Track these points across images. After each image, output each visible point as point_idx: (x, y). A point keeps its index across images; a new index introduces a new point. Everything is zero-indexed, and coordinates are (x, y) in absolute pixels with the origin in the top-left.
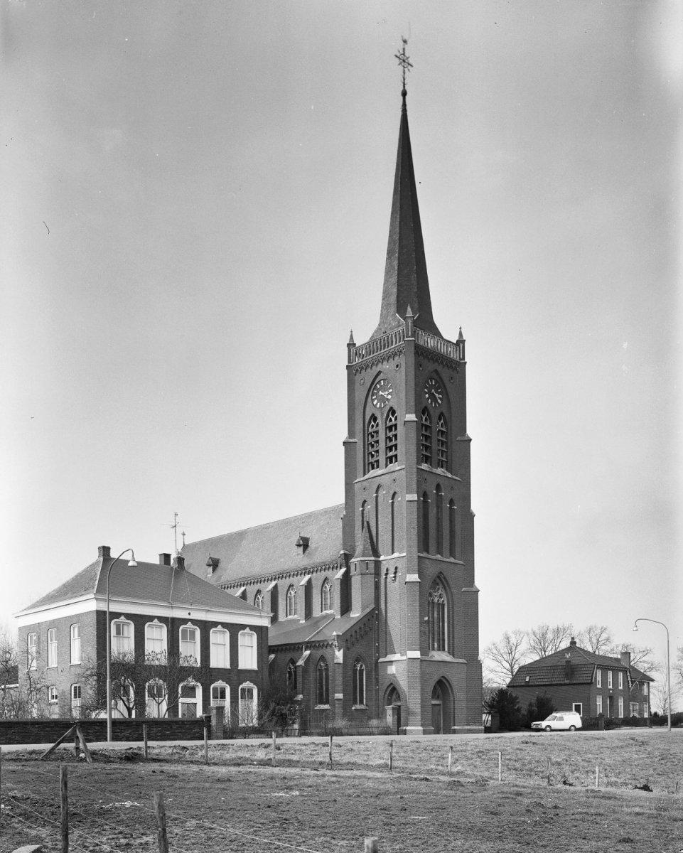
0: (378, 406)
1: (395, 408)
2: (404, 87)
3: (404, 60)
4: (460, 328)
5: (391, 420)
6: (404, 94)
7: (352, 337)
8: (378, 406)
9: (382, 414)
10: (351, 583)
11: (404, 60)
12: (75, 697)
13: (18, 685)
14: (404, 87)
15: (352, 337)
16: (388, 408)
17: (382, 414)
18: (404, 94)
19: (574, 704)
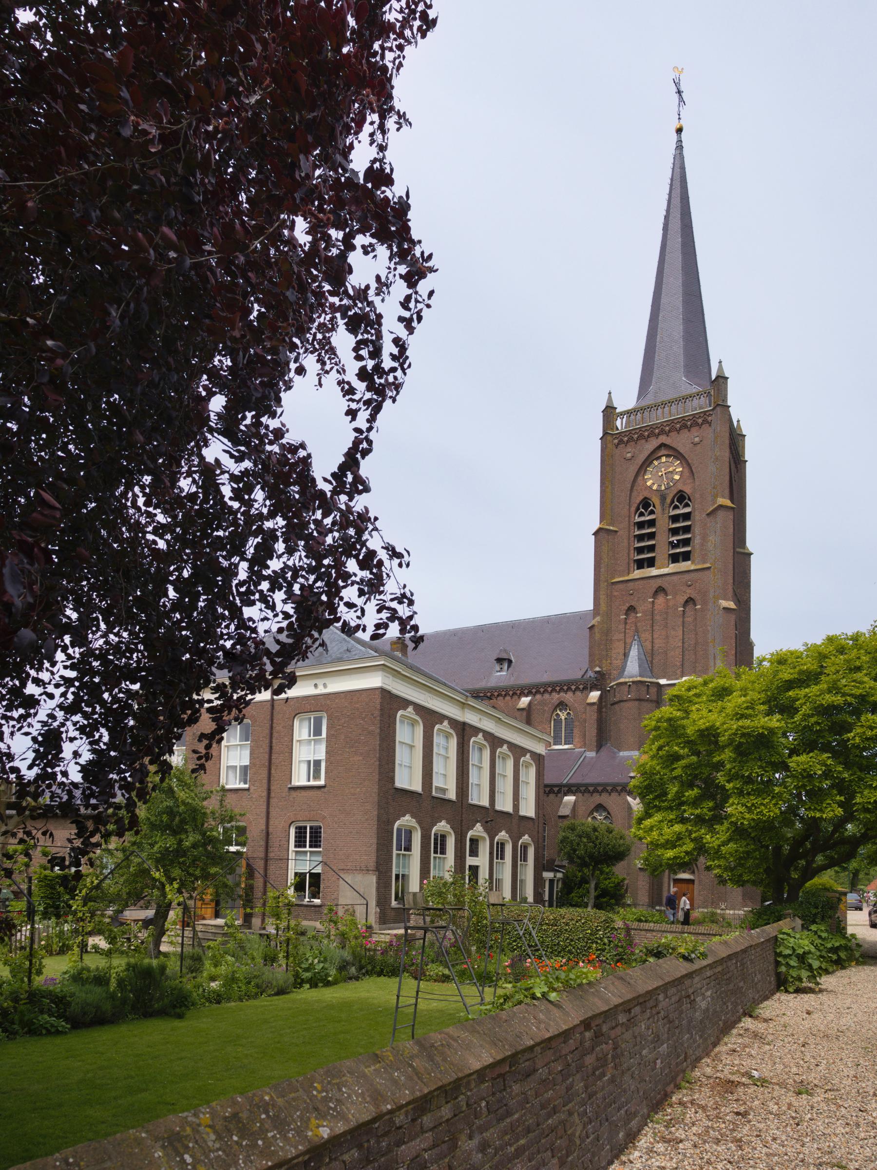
7: (610, 399)
15: (610, 399)
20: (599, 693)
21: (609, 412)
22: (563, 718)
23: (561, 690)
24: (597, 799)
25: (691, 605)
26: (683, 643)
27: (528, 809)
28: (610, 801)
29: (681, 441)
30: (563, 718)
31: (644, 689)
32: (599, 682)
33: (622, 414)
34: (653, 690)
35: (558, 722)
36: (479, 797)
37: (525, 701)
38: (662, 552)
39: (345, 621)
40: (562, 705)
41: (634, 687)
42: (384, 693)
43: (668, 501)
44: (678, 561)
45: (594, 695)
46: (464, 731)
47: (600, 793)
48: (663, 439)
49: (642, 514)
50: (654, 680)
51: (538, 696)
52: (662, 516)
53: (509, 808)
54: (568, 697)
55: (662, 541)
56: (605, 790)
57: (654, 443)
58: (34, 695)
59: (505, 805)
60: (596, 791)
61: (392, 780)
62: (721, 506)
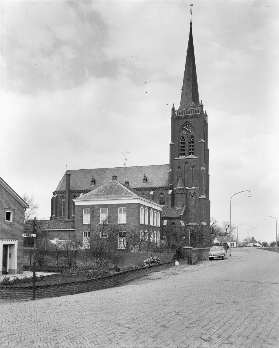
0: (185, 133)
1: (194, 135)
2: (191, 21)
3: (67, 166)
4: (206, 111)
5: (190, 139)
6: (191, 24)
7: (173, 106)
8: (185, 133)
9: (187, 137)
10: (10, 217)
11: (67, 166)
12: (85, 236)
13: (209, 257)
14: (191, 21)
15: (173, 106)
16: (190, 135)
17: (187, 137)
18: (191, 24)
19: (12, 212)
20: (171, 191)
21: (173, 110)
22: (162, 197)
23: (162, 189)
24: (172, 221)
25: (194, 167)
26: (192, 178)
27: (159, 225)
28: (176, 221)
29: (192, 121)
30: (162, 197)
31: (183, 190)
32: (171, 188)
33: (176, 111)
34: (185, 191)
35: (160, 198)
36: (151, 224)
37: (152, 193)
38: (187, 151)
39: (210, 249)
40: (162, 193)
41: (180, 190)
42: (139, 204)
43: (189, 137)
44: (191, 143)
45: (170, 192)
46: (149, 208)
47: (173, 219)
48: (187, 120)
49: (182, 140)
50: (185, 188)
51: (155, 191)
52: (187, 141)
53: (156, 225)
54: (163, 191)
55: (187, 147)
56: (174, 219)
57: (185, 121)
58: (53, 198)
59: (155, 225)
60: (172, 219)
61: (140, 222)
62: (201, 142)
